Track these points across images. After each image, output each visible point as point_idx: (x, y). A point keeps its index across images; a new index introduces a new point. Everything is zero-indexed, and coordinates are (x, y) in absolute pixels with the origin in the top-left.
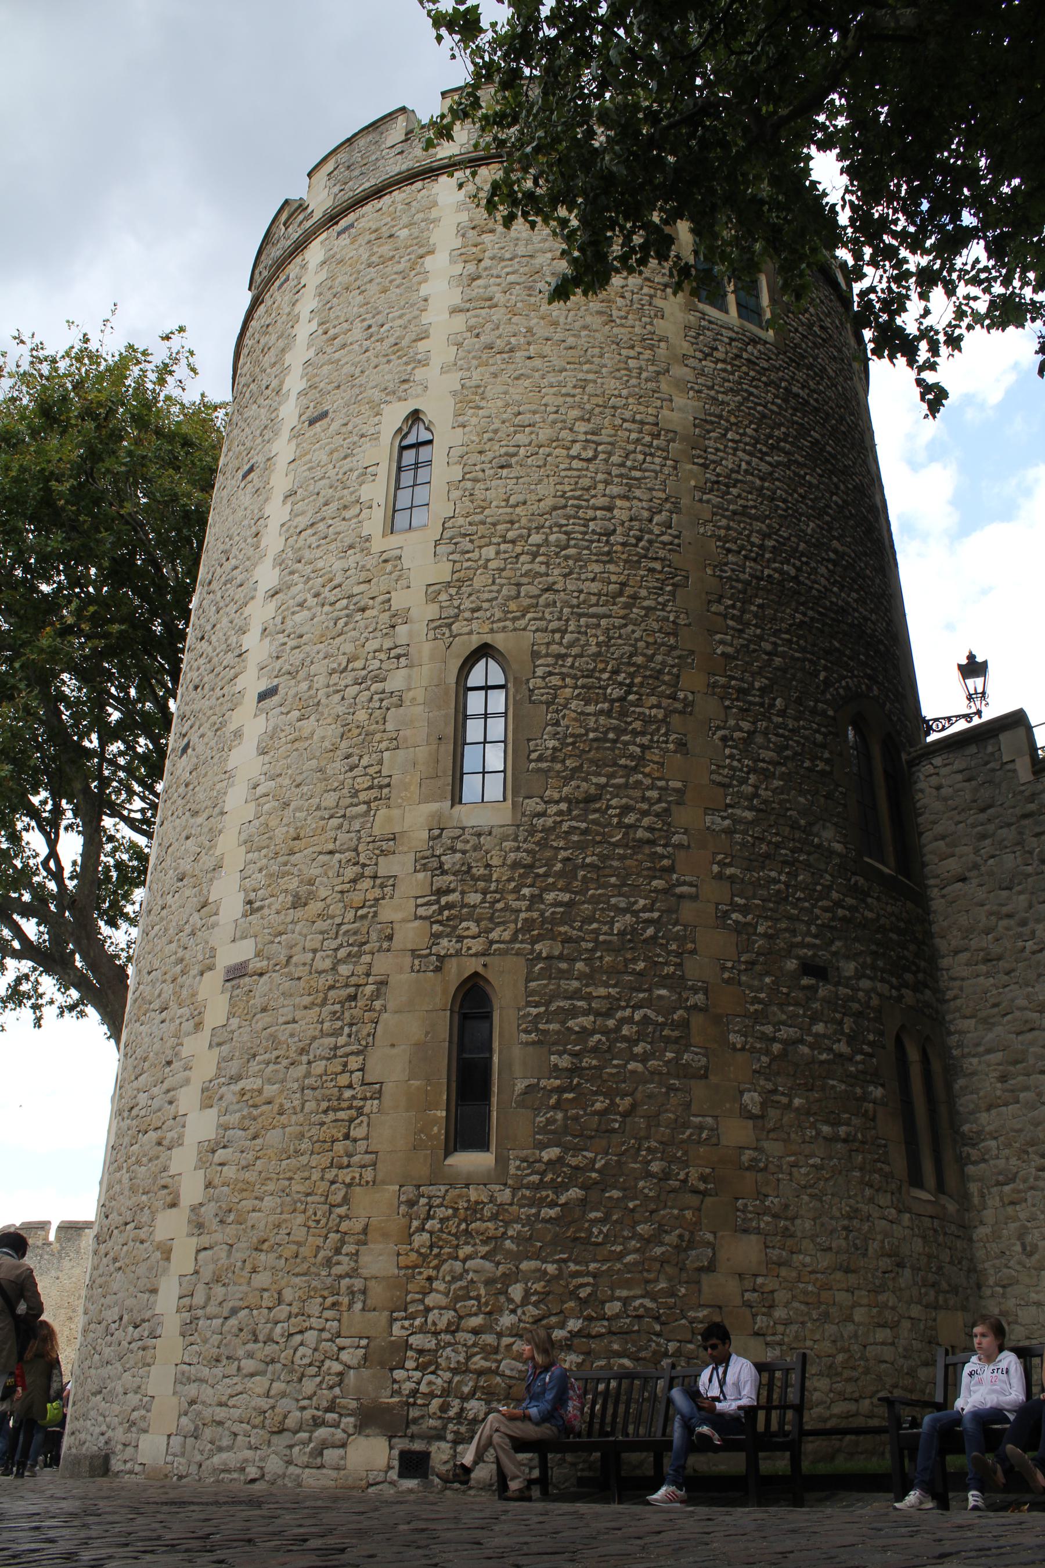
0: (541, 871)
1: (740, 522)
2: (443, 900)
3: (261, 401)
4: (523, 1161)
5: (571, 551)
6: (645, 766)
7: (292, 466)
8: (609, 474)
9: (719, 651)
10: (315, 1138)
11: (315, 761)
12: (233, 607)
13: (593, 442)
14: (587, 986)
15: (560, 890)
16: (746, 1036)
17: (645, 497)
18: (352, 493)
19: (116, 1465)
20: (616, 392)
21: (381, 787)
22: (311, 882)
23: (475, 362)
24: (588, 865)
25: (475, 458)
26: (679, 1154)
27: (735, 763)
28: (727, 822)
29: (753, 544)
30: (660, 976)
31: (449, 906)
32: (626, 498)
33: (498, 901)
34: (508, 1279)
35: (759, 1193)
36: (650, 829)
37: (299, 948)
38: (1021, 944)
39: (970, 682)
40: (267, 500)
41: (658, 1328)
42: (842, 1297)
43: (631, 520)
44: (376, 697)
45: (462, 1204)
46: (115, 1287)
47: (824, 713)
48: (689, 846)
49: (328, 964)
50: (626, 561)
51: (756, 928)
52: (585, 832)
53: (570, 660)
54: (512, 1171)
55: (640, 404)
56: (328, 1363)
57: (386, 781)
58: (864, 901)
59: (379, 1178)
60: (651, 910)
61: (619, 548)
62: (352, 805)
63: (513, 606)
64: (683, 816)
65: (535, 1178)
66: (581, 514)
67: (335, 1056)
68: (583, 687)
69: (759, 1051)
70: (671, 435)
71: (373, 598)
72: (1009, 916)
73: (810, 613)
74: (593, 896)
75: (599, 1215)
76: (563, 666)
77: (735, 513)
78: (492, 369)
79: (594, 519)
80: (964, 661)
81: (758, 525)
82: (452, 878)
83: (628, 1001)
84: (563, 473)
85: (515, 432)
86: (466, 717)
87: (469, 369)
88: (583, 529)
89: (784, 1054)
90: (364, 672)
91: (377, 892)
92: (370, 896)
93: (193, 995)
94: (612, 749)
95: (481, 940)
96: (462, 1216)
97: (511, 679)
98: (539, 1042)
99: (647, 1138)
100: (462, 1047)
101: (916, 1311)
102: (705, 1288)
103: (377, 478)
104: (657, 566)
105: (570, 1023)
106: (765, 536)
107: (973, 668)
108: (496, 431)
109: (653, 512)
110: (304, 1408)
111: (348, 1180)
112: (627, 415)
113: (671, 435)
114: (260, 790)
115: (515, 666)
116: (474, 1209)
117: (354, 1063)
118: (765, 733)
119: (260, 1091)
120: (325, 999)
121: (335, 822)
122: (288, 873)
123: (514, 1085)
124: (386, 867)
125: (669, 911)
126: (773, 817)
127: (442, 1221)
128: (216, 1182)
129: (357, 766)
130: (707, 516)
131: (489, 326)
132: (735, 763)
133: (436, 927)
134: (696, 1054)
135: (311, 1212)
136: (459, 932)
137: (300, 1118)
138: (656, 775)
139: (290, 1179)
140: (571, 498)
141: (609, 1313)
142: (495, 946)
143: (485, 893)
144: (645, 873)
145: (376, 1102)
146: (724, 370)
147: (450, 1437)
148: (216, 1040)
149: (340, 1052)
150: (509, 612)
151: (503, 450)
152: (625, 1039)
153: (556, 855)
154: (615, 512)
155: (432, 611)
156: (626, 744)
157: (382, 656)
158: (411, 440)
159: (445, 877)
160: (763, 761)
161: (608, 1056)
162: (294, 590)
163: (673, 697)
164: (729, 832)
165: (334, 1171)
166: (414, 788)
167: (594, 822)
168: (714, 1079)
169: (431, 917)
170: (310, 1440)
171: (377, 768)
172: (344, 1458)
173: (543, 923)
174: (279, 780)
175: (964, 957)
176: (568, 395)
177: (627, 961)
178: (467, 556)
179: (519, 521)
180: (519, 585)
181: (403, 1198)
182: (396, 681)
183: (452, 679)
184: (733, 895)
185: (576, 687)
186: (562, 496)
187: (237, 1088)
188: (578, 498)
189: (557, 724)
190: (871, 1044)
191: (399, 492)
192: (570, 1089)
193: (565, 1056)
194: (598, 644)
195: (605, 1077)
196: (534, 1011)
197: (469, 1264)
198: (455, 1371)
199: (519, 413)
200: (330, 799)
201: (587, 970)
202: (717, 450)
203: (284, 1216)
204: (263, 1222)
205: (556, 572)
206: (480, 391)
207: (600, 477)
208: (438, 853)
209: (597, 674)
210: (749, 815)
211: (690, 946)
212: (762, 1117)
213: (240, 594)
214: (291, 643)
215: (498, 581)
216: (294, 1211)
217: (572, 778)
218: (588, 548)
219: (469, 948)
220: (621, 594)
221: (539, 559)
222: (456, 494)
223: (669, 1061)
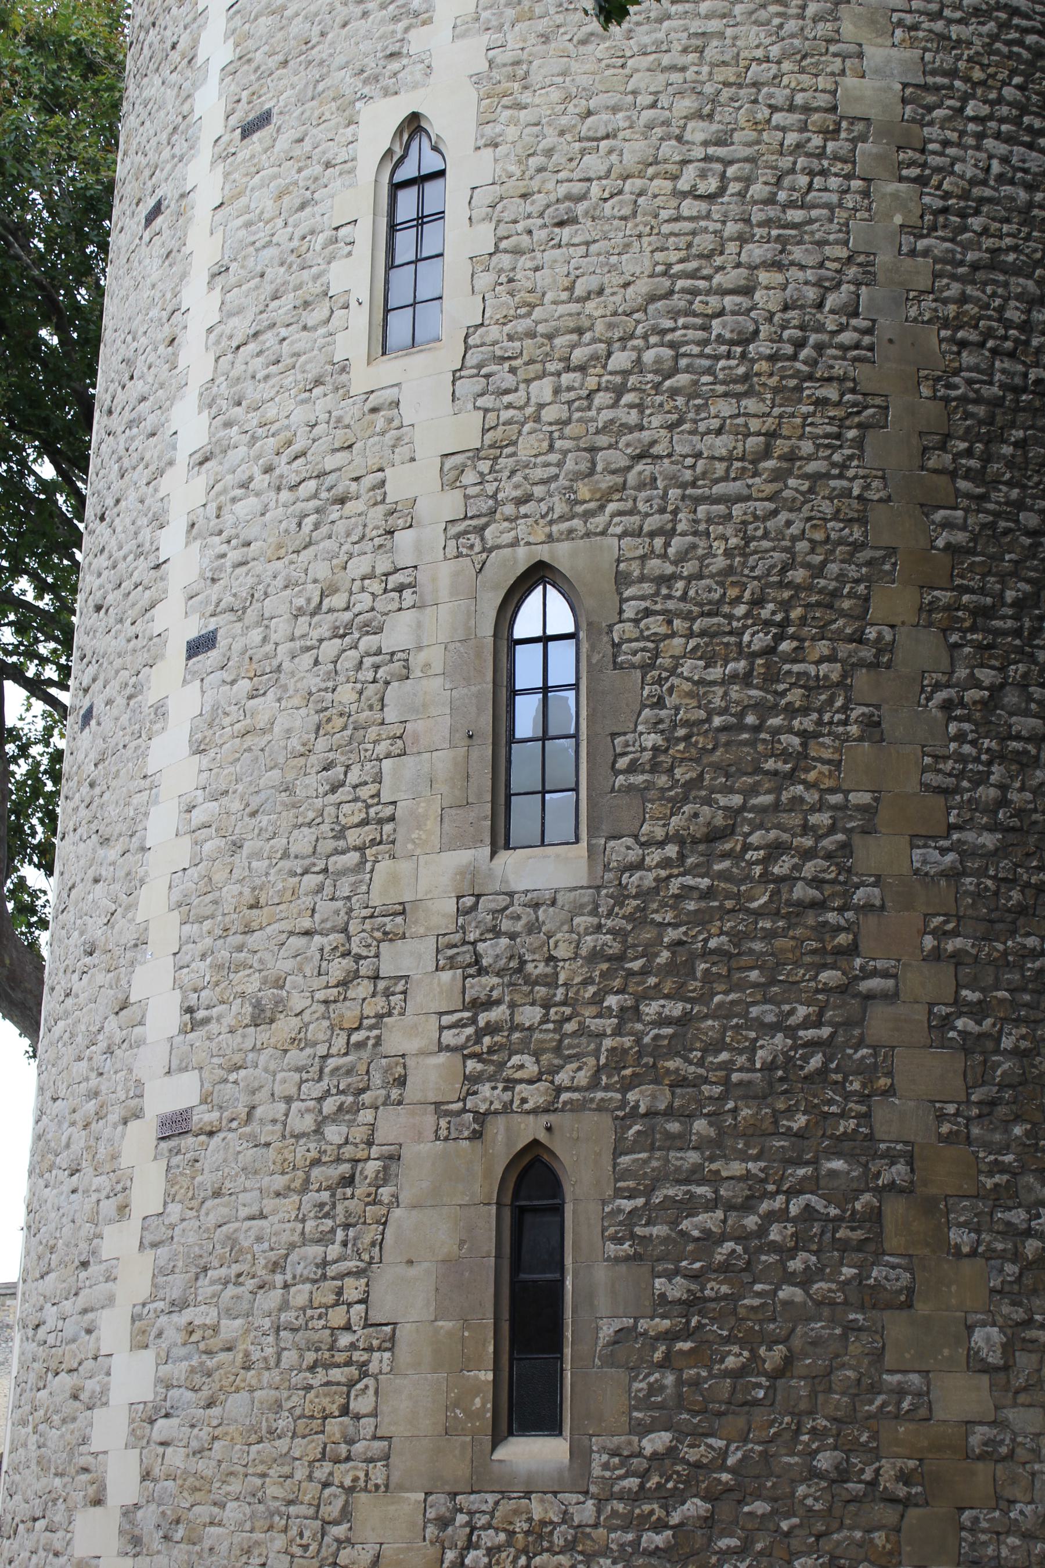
0: (636, 965)
1: (985, 284)
2: (482, 1019)
3: (165, 71)
4: (613, 1454)
5: (682, 379)
6: (807, 770)
7: (221, 212)
8: (747, 221)
9: (940, 543)
10: (298, 1412)
11: (276, 772)
12: (141, 475)
13: (718, 160)
14: (712, 1159)
15: (667, 997)
16: (978, 1232)
18: (316, 278)
20: (759, 53)
21: (381, 822)
22: (279, 983)
24: (713, 952)
25: (514, 208)
26: (864, 1438)
27: (967, 749)
28: (951, 857)
29: (1008, 324)
30: (832, 1137)
31: (491, 1029)
32: (776, 265)
33: (569, 1019)
35: (998, 1498)
36: (816, 882)
40: (184, 276)
43: (786, 308)
44: (368, 661)
45: (521, 1525)
48: (883, 907)
49: (308, 1123)
50: (776, 390)
51: (998, 1041)
52: (708, 894)
53: (680, 585)
54: (597, 1471)
55: (802, 71)
57: (388, 811)
59: (394, 1479)
60: (818, 1024)
61: (763, 366)
62: (337, 852)
63: (584, 491)
64: (875, 854)
65: (632, 1483)
66: (697, 306)
67: (324, 1277)
68: (703, 634)
69: (1002, 1256)
70: (859, 127)
71: (356, 479)
74: (721, 1005)
75: (734, 1542)
76: (669, 597)
77: (975, 267)
78: (541, 25)
79: (721, 313)
81: (1021, 284)
82: (495, 980)
83: (779, 1183)
84: (666, 228)
85: (583, 152)
86: (513, 693)
88: (700, 334)
90: (347, 616)
91: (379, 1004)
92: (369, 1011)
93: (114, 1157)
94: (752, 743)
95: (542, 1086)
96: (520, 1545)
97: (584, 625)
98: (636, 1257)
99: (811, 1413)
100: (516, 1265)
103: (356, 250)
104: (831, 392)
105: (685, 1225)
108: (549, 153)
109: (825, 287)
111: (348, 1483)
113: (859, 127)
114: (198, 816)
117: (353, 1289)
118: (1023, 686)
119: (215, 1329)
120: (307, 1181)
121: (311, 881)
122: (245, 966)
123: (598, 1329)
124: (395, 960)
125: (848, 1024)
126: (1032, 839)
127: (490, 1551)
128: (156, 1472)
129: (342, 784)
130: (924, 282)
132: (967, 749)
133: (472, 1065)
134: (893, 1267)
135: (293, 1532)
136: (507, 1073)
137: (275, 1376)
138: (827, 783)
139: (264, 1475)
142: (565, 1096)
143: (546, 1006)
144: (808, 959)
145: (387, 1355)
148: (149, 1238)
149: (331, 1271)
150: (577, 502)
151: (562, 190)
152: (775, 1247)
153: (660, 936)
154: (757, 295)
155: (451, 504)
156: (776, 732)
157: (376, 586)
159: (484, 980)
160: (1018, 737)
161: (746, 1278)
162: (235, 456)
163: (858, 638)
164: (953, 875)
165: (327, 1466)
166: (432, 824)
167: (723, 876)
168: (922, 1308)
169: (464, 1047)
171: (372, 788)
173: (640, 1055)
174: (224, 800)
176: (673, 68)
177: (776, 1115)
178: (507, 399)
179: (591, 328)
180: (593, 450)
181: (431, 1514)
182: (398, 634)
183: (487, 629)
184: (959, 987)
185: (690, 635)
186: (665, 274)
188: (693, 275)
189: (660, 704)
191: (393, 272)
192: (686, 1333)
193: (678, 1279)
194: (728, 553)
195: (742, 1312)
196: (627, 1205)
199: (589, 113)
200: (303, 841)
201: (712, 1132)
202: (946, 143)
203: (258, 1536)
204: (226, 1545)
205: (656, 421)
206: (520, 73)
207: (732, 228)
208: (471, 937)
209: (726, 609)
210: (989, 840)
211: (883, 1082)
212: (1006, 1368)
213: (152, 450)
214: (234, 556)
215: (558, 444)
216: (270, 1528)
217: (685, 800)
218: (710, 371)
219: (524, 1101)
220: (766, 453)
221: (628, 398)
222: (484, 280)
223: (847, 1282)
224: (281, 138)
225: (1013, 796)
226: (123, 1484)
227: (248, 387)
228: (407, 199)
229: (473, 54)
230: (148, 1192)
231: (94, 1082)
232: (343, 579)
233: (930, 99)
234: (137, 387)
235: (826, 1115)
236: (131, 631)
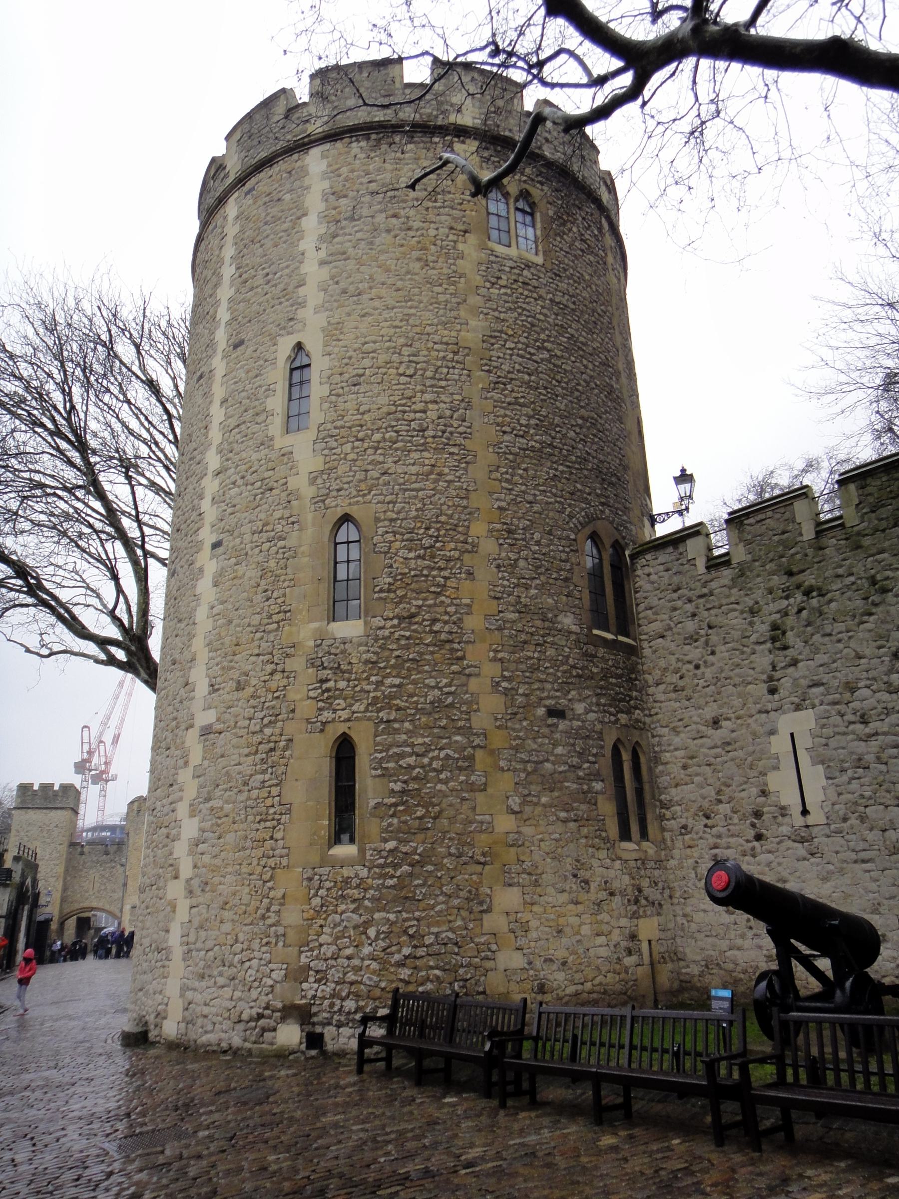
0: (382, 665)
2: (324, 686)
5: (400, 445)
17: (448, 400)
19: (152, 1035)
21: (286, 612)
23: (335, 304)
25: (337, 378)
27: (505, 583)
29: (521, 425)
31: (328, 690)
32: (436, 402)
34: (367, 924)
37: (240, 717)
38: (696, 681)
39: (682, 487)
40: (211, 402)
41: (456, 950)
42: (574, 920)
43: (439, 418)
46: (148, 924)
47: (568, 537)
54: (368, 857)
56: (264, 980)
58: (591, 661)
60: (450, 686)
61: (430, 440)
63: (363, 486)
65: (382, 861)
66: (406, 417)
69: (519, 770)
72: (689, 662)
73: (561, 468)
75: (420, 882)
77: (509, 404)
78: (347, 309)
80: (678, 474)
81: (525, 410)
84: (394, 387)
86: (336, 563)
87: (331, 310)
89: (535, 770)
92: (281, 684)
93: (183, 743)
94: (426, 581)
98: (383, 775)
101: (624, 922)
102: (485, 923)
104: (455, 450)
105: (401, 763)
106: (530, 417)
107: (684, 478)
108: (350, 358)
109: (454, 410)
110: (252, 1008)
112: (437, 338)
114: (215, 611)
115: (364, 528)
116: (347, 881)
119: (222, 808)
121: (258, 635)
122: (233, 668)
124: (290, 665)
128: (199, 865)
130: (490, 409)
131: (345, 275)
132: (505, 583)
133: (321, 704)
140: (401, 405)
141: (427, 943)
143: (349, 681)
146: (506, 294)
147: (334, 1022)
152: (435, 770)
156: (434, 577)
157: (284, 522)
158: (297, 364)
164: (500, 629)
168: (490, 790)
170: (256, 1027)
171: (282, 599)
172: (275, 1038)
175: (662, 687)
181: (305, 876)
182: (291, 542)
185: (403, 541)
187: (208, 805)
188: (403, 405)
189: (391, 566)
190: (594, 755)
192: (403, 803)
196: (379, 756)
197: (344, 916)
198: (337, 983)
199: (366, 343)
200: (256, 619)
201: (411, 727)
202: (499, 357)
205: (390, 460)
207: (419, 388)
211: (475, 707)
213: (199, 469)
214: (230, 510)
217: (400, 603)
218: (410, 441)
220: (431, 473)
221: (379, 451)
224: (247, 351)
225: (523, 600)
226: (186, 869)
227: (235, 445)
228: (297, 374)
229: (321, 320)
230: (196, 755)
231: (175, 714)
232: (271, 519)
233: (493, 341)
234: (193, 445)
235: (453, 720)
236: (190, 539)
